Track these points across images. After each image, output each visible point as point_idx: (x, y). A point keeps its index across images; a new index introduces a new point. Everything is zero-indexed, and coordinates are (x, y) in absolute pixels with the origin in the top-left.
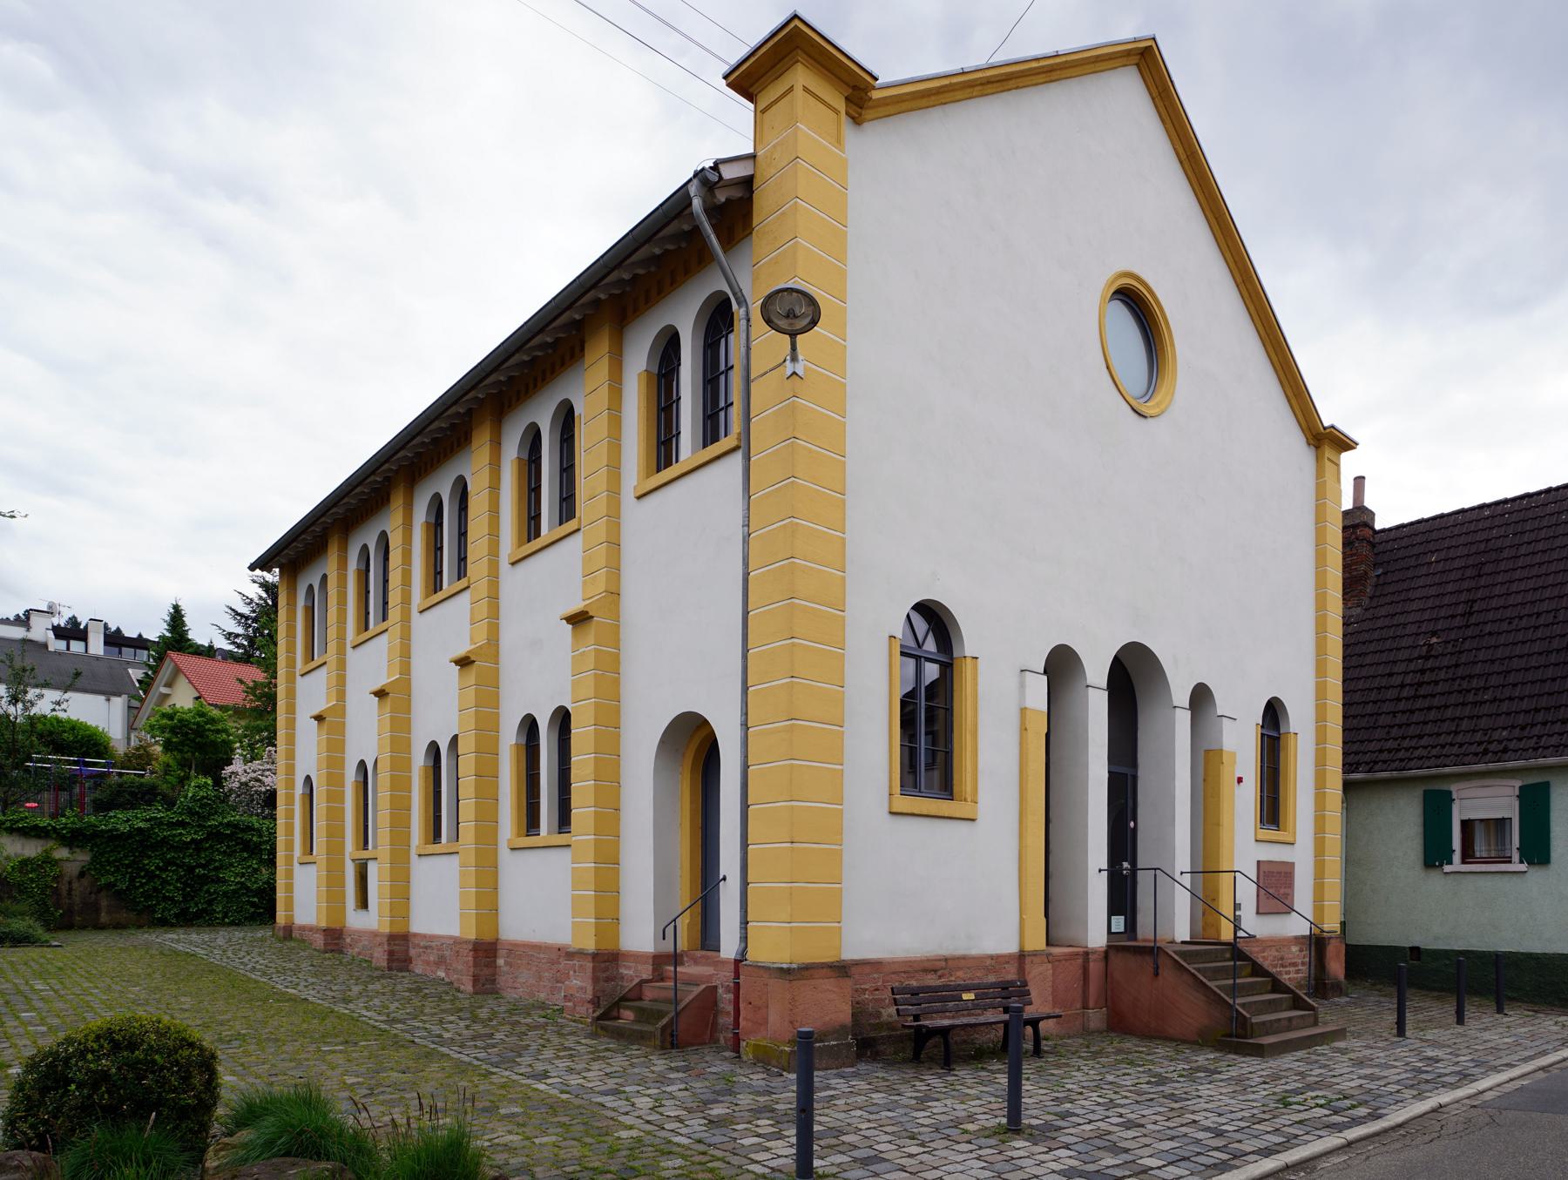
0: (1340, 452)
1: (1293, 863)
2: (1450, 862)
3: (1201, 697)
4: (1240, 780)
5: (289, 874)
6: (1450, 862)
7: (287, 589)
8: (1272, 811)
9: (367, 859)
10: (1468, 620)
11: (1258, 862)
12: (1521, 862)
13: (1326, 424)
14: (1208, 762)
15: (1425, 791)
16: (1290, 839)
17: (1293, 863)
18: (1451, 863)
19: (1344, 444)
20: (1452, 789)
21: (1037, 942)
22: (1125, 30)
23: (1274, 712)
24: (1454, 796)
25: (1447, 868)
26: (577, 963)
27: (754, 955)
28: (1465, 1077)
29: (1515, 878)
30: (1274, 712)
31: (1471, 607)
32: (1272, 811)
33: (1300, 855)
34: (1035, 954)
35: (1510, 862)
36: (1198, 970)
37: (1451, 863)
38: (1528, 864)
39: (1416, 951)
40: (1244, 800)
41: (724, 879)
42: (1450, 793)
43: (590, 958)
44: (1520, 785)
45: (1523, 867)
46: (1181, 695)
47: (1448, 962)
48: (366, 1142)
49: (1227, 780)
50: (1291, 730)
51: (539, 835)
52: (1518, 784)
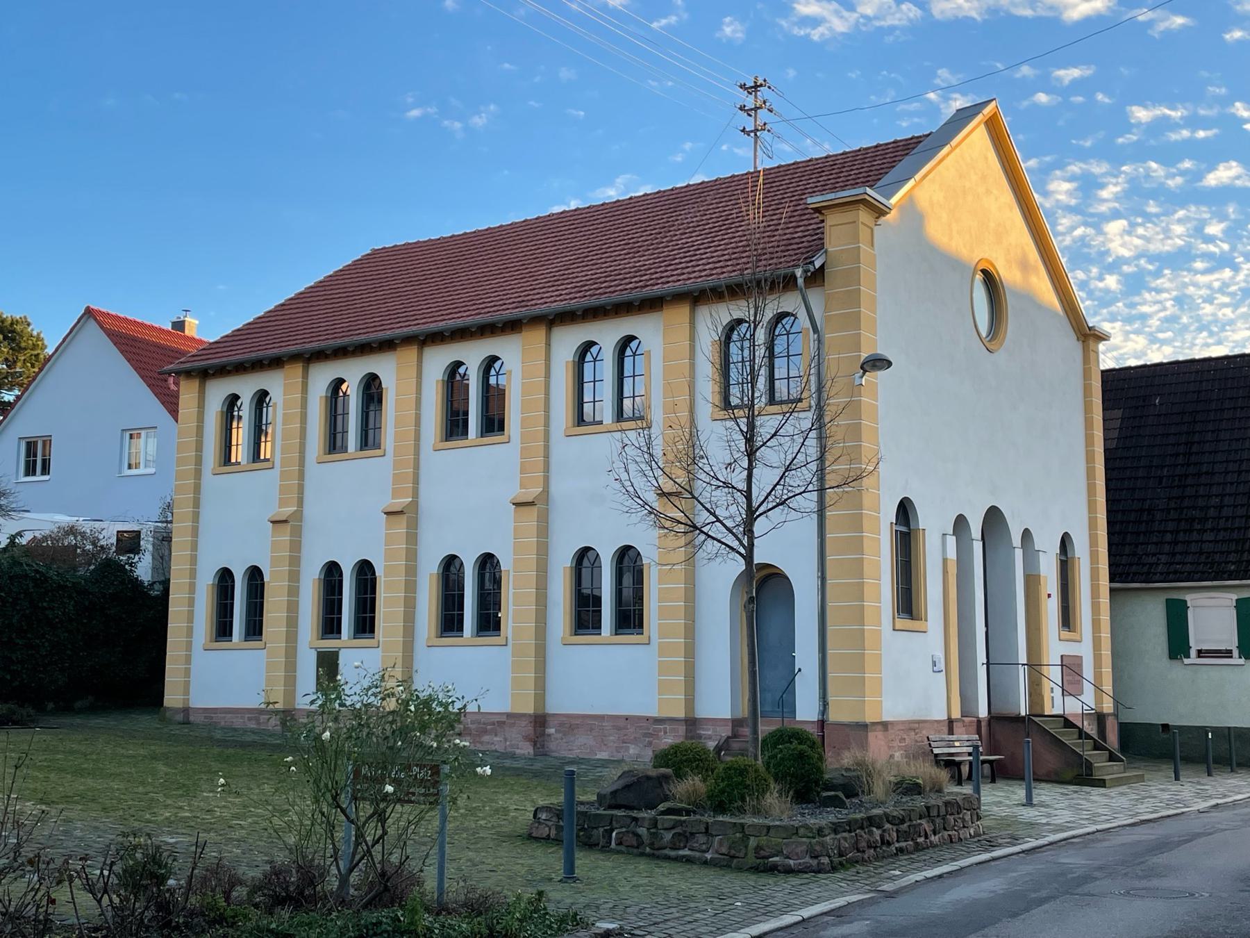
0: (1098, 343)
1: (1082, 657)
2: (1188, 656)
3: (1027, 534)
4: (1049, 596)
5: (188, 660)
6: (1188, 656)
7: (199, 393)
8: (1067, 619)
9: (340, 648)
10: (1188, 459)
11: (1062, 656)
12: (1240, 657)
13: (1090, 325)
14: (1032, 581)
15: (1167, 600)
16: (1078, 638)
17: (1082, 657)
18: (1189, 657)
19: (1101, 337)
20: (1186, 599)
21: (956, 714)
22: (896, 632)
23: (1065, 542)
24: (1189, 604)
25: (1186, 661)
26: (668, 727)
27: (834, 716)
28: (1225, 796)
29: (1236, 669)
30: (1065, 542)
31: (1190, 448)
32: (1067, 619)
33: (1084, 650)
34: (957, 720)
35: (1231, 657)
36: (1056, 732)
37: (1189, 657)
38: (1245, 659)
39: (1166, 727)
40: (1051, 609)
41: (800, 670)
42: (1186, 601)
43: (684, 722)
44: (1236, 598)
45: (1242, 661)
46: (1016, 540)
47: (1190, 736)
48: (420, 883)
49: (1044, 596)
50: (1076, 556)
51: (600, 634)
52: (1235, 597)
